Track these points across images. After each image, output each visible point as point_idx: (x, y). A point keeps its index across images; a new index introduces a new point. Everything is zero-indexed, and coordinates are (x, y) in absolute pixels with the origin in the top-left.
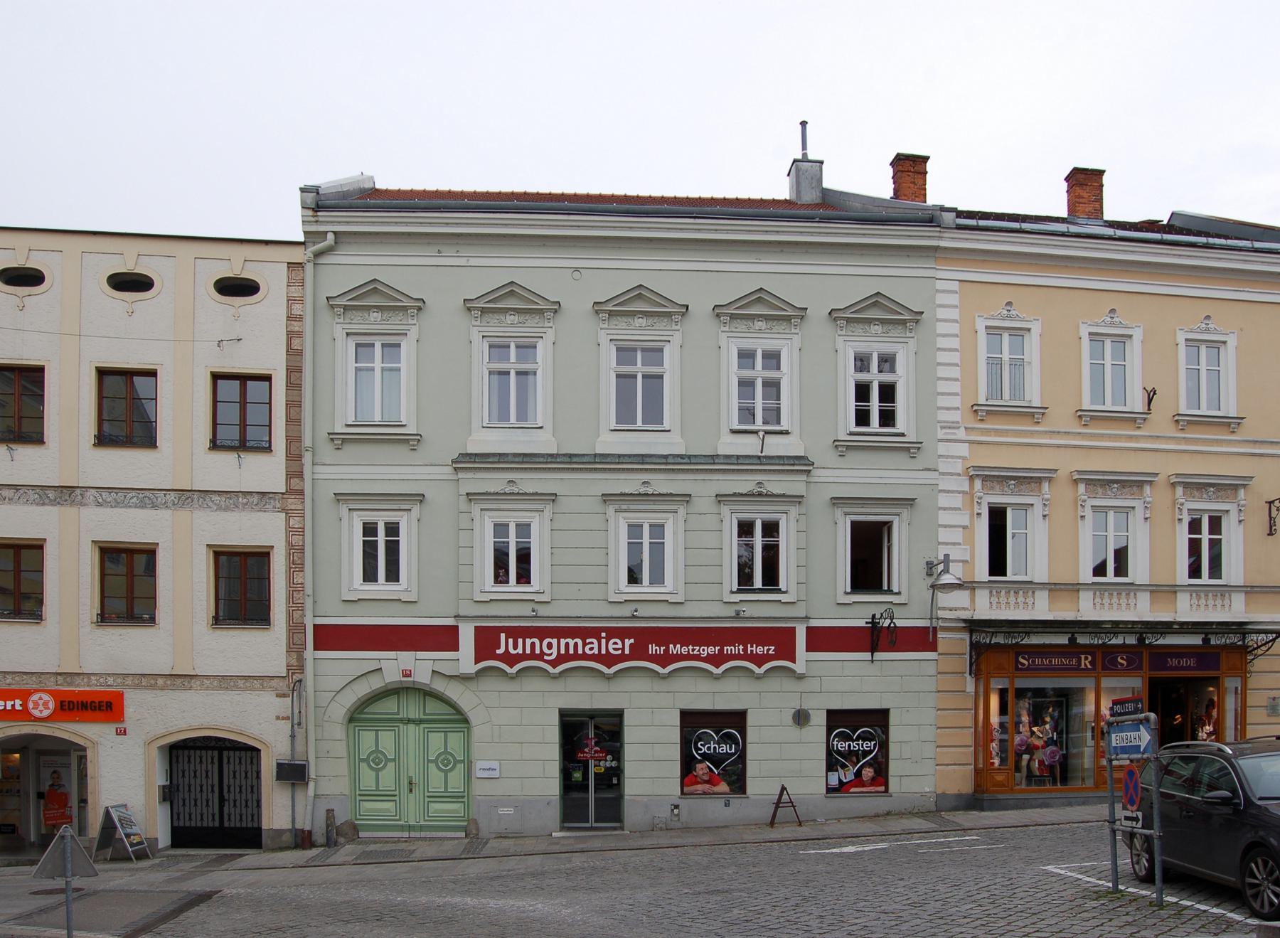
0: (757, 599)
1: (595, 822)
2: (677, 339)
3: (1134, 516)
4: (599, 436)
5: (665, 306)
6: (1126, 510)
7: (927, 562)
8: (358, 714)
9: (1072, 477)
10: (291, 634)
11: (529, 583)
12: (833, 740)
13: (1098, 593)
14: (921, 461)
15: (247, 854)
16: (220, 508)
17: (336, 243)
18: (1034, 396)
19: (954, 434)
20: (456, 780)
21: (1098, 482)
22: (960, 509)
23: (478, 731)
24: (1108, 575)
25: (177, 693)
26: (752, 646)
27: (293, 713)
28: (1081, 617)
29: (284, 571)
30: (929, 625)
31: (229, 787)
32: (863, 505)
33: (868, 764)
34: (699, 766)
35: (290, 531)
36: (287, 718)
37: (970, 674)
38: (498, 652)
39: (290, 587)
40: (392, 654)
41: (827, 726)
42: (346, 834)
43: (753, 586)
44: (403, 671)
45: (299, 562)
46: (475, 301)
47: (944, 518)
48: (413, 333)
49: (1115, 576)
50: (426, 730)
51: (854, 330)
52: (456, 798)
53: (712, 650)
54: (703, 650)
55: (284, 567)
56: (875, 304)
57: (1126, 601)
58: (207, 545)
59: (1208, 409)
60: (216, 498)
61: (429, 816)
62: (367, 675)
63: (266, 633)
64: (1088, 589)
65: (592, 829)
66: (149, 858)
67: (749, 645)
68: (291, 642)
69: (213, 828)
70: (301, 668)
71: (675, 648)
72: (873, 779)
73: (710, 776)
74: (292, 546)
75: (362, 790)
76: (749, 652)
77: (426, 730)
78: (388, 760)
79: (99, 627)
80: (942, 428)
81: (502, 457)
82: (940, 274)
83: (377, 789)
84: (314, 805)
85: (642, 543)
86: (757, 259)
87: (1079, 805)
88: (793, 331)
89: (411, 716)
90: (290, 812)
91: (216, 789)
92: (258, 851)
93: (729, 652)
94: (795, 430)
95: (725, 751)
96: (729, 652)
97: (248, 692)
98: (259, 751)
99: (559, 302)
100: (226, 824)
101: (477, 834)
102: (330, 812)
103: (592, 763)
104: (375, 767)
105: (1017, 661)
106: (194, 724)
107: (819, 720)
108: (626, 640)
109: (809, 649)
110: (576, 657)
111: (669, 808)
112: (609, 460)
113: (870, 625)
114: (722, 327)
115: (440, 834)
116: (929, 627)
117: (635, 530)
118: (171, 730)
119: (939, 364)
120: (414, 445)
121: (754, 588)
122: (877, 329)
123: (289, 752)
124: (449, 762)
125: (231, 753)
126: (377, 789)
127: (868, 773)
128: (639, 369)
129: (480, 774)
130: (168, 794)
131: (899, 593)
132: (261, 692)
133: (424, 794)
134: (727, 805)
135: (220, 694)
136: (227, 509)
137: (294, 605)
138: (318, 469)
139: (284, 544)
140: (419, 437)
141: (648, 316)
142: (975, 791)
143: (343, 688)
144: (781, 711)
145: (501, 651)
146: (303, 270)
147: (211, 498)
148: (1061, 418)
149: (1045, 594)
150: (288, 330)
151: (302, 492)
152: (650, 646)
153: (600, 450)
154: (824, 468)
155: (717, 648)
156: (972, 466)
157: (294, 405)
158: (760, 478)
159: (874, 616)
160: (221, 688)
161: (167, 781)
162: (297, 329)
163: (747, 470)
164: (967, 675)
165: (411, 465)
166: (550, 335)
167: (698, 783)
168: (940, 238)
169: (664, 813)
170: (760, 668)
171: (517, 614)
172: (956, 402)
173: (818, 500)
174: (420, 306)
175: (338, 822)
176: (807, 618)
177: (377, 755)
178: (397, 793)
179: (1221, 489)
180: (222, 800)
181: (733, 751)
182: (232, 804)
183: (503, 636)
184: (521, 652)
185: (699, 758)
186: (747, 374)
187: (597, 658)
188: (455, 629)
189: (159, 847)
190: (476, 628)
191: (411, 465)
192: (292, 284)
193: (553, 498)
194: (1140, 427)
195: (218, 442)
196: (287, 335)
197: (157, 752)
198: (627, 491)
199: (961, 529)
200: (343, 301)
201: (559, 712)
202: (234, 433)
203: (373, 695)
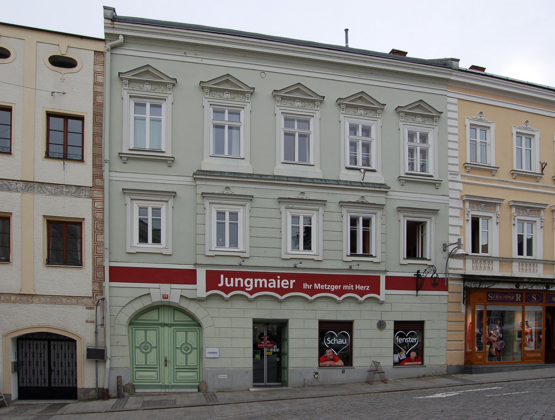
0: (361, 260)
1: (267, 382)
2: (318, 115)
3: (535, 225)
4: (276, 166)
6: (532, 223)
7: (444, 244)
8: (134, 320)
9: (509, 204)
10: (95, 272)
11: (311, 249)
12: (396, 338)
13: (521, 263)
14: (441, 191)
15: (69, 403)
16: (51, 194)
17: (124, 42)
18: (492, 161)
19: (456, 178)
20: (192, 359)
21: (522, 207)
22: (458, 217)
23: (207, 331)
24: (533, 255)
25: (24, 306)
26: (358, 286)
27: (96, 319)
28: (514, 275)
29: (91, 234)
30: (445, 277)
31: (54, 363)
32: (413, 212)
33: (413, 350)
34: (328, 351)
35: (95, 210)
36: (93, 322)
37: (463, 303)
38: (219, 285)
39: (95, 244)
40: (157, 285)
41: (394, 330)
42: (129, 391)
44: (163, 295)
45: (100, 229)
46: (207, 83)
47: (452, 221)
48: (170, 99)
49: (527, 255)
50: (175, 330)
51: (408, 119)
52: (192, 369)
53: (337, 287)
54: (332, 287)
55: (91, 231)
56: (418, 106)
57: (533, 268)
58: (43, 216)
59: (526, 169)
60: (49, 187)
61: (176, 380)
62: (141, 297)
63: (80, 270)
64: (517, 261)
65: (265, 386)
66: (6, 406)
67: (356, 285)
69: (45, 387)
70: (102, 292)
71: (317, 286)
72: (416, 358)
73: (334, 357)
74: (96, 219)
75: (137, 365)
76: (356, 289)
77: (175, 330)
78: (152, 347)
79: (48, 267)
80: (450, 174)
81: (222, 174)
82: (449, 94)
84: (110, 373)
85: (160, 220)
86: (359, 76)
87: (515, 370)
88: (316, 109)
89: (166, 322)
90: (95, 378)
91: (47, 364)
92: (75, 401)
93: (346, 289)
94: (379, 169)
95: (341, 343)
96: (346, 289)
97: (68, 306)
98: (75, 341)
99: (176, 79)
100: (53, 385)
101: (206, 390)
102: (119, 378)
103: (265, 350)
105: (488, 297)
106: (35, 325)
107: (390, 326)
108: (291, 281)
109: (387, 288)
110: (263, 289)
111: (313, 374)
112: (282, 179)
113: (416, 276)
114: (341, 111)
115: (183, 390)
116: (445, 278)
117: (221, 215)
118: (20, 328)
119: (449, 141)
120: (170, 164)
121: (370, 254)
123: (94, 342)
124: (188, 349)
125: (56, 343)
127: (413, 355)
128: (296, 129)
129: (208, 355)
130: (17, 367)
131: (430, 260)
132: (77, 306)
134: (343, 372)
135: (51, 306)
136: (55, 194)
137: (97, 254)
138: (113, 174)
139: (91, 217)
140: (173, 159)
141: (365, 109)
142: (465, 363)
143: (127, 304)
144: (371, 321)
146: (104, 56)
147: (46, 187)
148: (504, 174)
149: (498, 263)
150: (94, 90)
151: (102, 188)
152: (304, 284)
153: (276, 173)
154: (394, 191)
155: (340, 286)
156: (513, 201)
157: (98, 135)
158: (363, 194)
159: (418, 272)
160: (51, 303)
161: (16, 359)
162: (99, 90)
163: (356, 189)
164: (462, 304)
166: (248, 107)
167: (327, 360)
168: (451, 75)
169: (310, 377)
170: (282, 296)
171: (231, 264)
172: (456, 161)
173: (391, 207)
174: (174, 83)
175: (124, 384)
176: (386, 271)
177: (146, 344)
178: (158, 366)
179: (488, 205)
180: (50, 371)
181: (346, 343)
182: (56, 373)
183: (222, 276)
184: (232, 286)
185: (328, 346)
186: (289, 130)
187: (275, 290)
188: (194, 272)
189: (12, 400)
190: (207, 271)
192: (97, 64)
193: (250, 198)
194: (538, 181)
195: (50, 154)
196: (94, 93)
197: (10, 341)
198: (292, 197)
199: (459, 228)
200: (129, 76)
201: (253, 320)
202: (61, 149)
203: (145, 309)
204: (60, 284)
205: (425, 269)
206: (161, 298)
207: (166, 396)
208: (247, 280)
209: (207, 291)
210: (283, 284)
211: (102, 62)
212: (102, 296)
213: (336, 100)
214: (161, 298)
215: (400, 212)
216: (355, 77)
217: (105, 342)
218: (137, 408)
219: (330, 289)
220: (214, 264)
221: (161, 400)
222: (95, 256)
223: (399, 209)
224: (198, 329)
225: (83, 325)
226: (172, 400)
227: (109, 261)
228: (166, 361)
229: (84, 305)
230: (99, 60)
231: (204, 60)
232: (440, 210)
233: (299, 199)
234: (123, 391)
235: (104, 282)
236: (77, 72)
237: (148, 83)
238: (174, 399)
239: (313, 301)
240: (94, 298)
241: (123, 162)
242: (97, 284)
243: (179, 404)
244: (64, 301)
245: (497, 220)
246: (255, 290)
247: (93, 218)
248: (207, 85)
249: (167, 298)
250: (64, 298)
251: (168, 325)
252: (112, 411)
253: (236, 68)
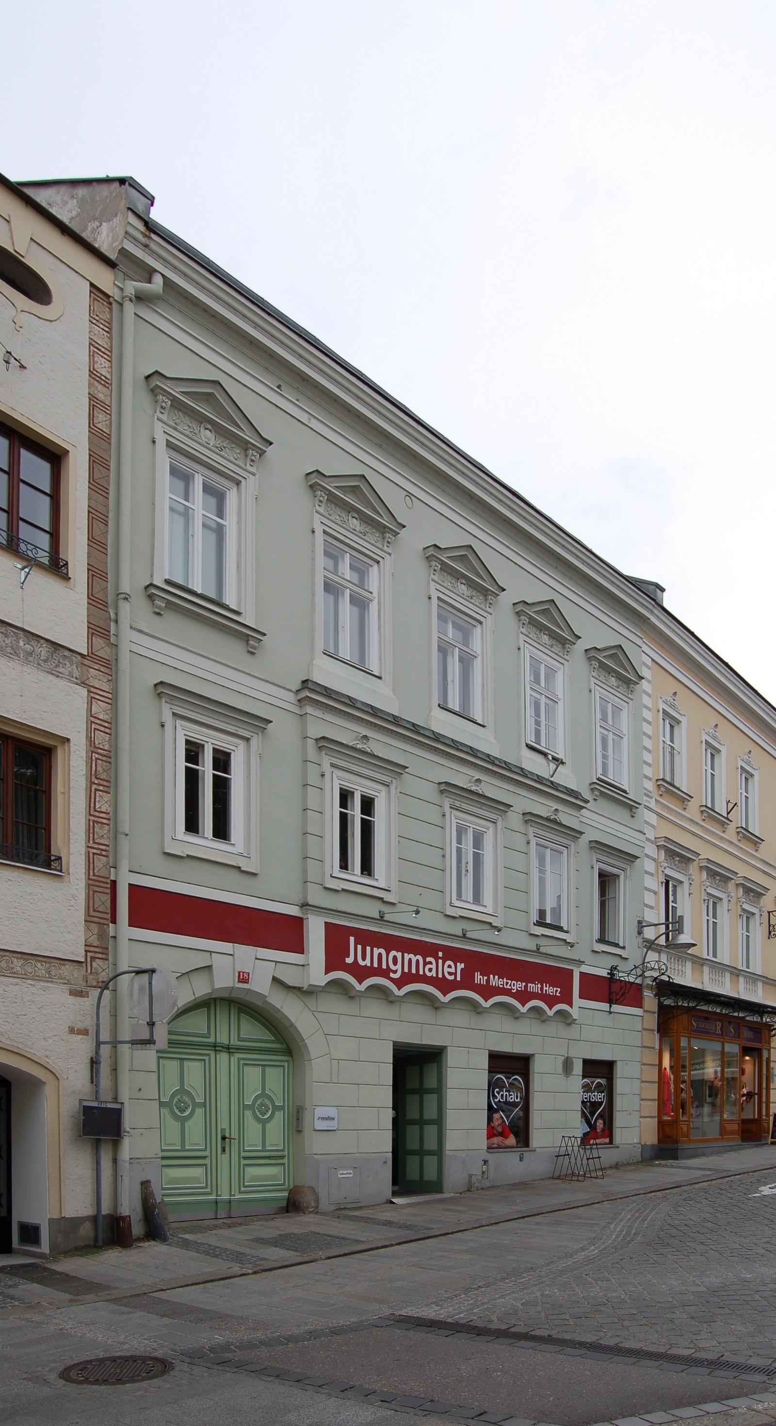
5: (484, 580)
10: (91, 893)
26: (546, 987)
36: (85, 1032)
44: (239, 973)
45: (104, 776)
68: (91, 906)
77: (242, 1062)
83: (183, 1149)
94: (489, 722)
97: (30, 982)
101: (317, 1207)
104: (179, 1114)
107: (578, 1068)
122: (545, 639)
129: (320, 1125)
131: (624, 948)
132: (49, 984)
133: (239, 1154)
137: (96, 846)
142: (659, 1141)
145: (349, 960)
152: (476, 973)
156: (708, 859)
159: (614, 968)
164: (656, 1032)
165: (249, 674)
168: (652, 612)
183: (352, 939)
191: (249, 674)
200: (176, 391)
201: (394, 1046)
204: (10, 916)
205: (635, 965)
206: (234, 980)
208: (393, 953)
209: (327, 971)
210: (446, 970)
211: (105, 321)
212: (106, 962)
213: (307, 472)
214: (234, 980)
215: (592, 851)
216: (460, 513)
219: (510, 987)
222: (90, 850)
223: (594, 845)
224: (287, 1061)
225: (62, 1040)
228: (224, 1138)
229: (65, 984)
230: (98, 314)
231: (313, 420)
232: (639, 858)
233: (471, 791)
236: (51, 321)
237: (210, 427)
239: (321, 989)
240: (86, 965)
241: (156, 610)
242: (95, 929)
244: (19, 969)
245: (690, 890)
246: (406, 979)
247: (88, 743)
248: (326, 484)
250: (17, 958)
253: (372, 471)
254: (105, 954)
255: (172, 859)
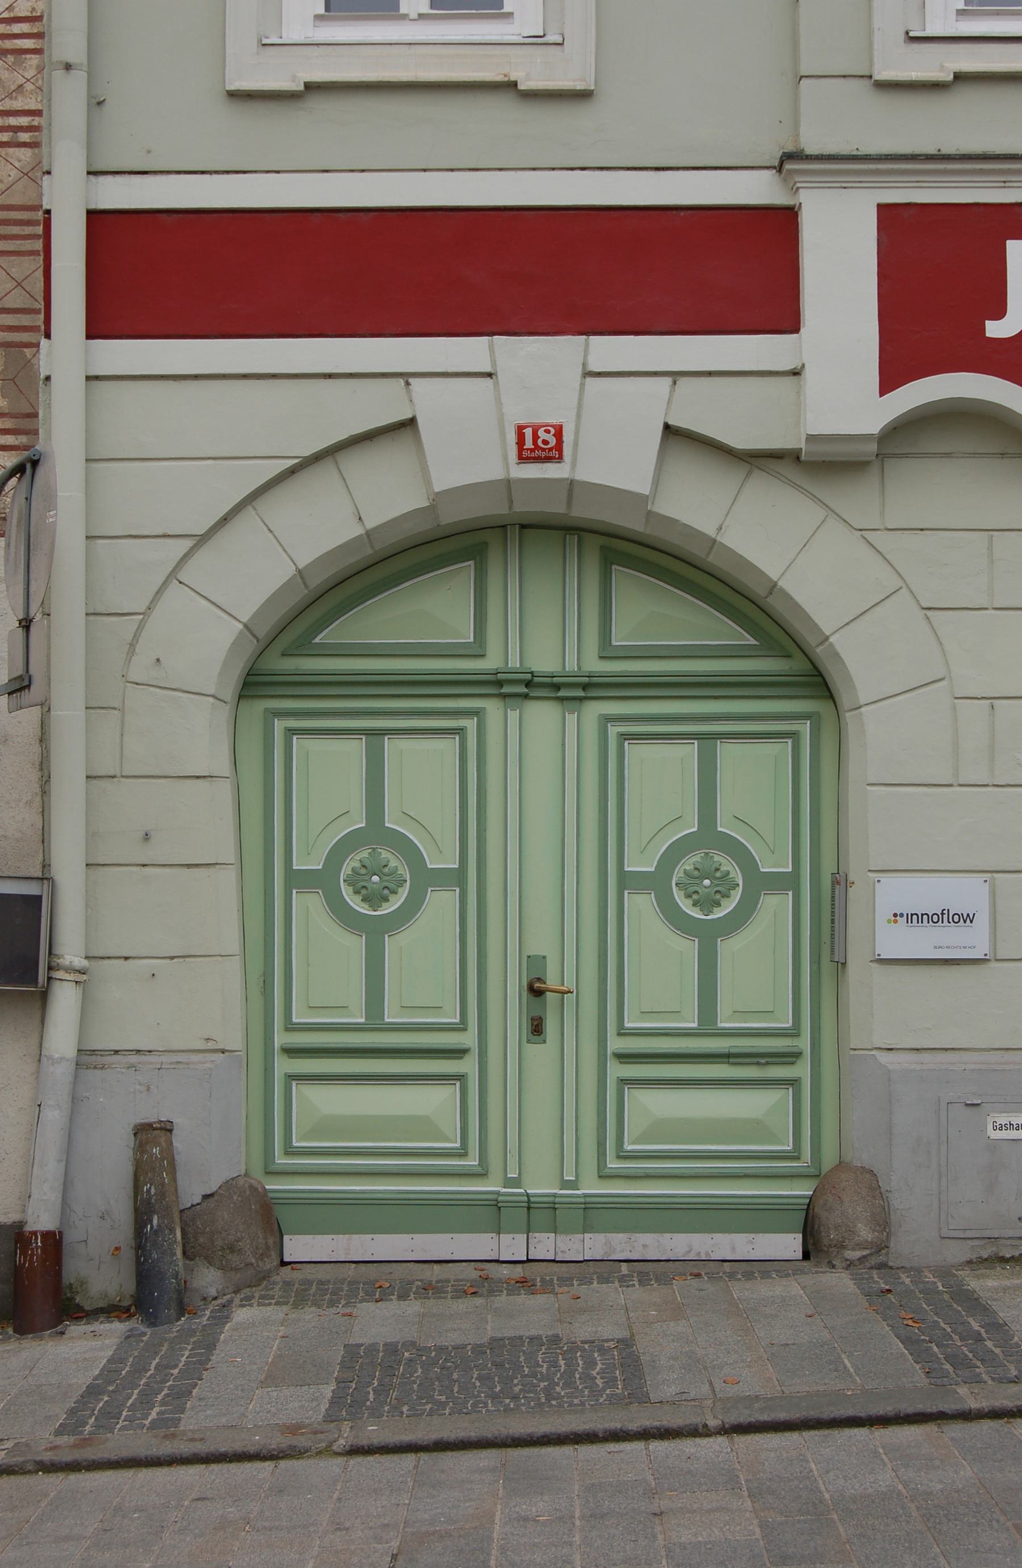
42: (232, 1249)
43: (502, 8)
44: (520, 430)
50: (613, 730)
61: (622, 1156)
77: (613, 730)
83: (375, 1022)
84: (75, 1100)
101: (880, 1247)
104: (696, 914)
124: (724, 886)
126: (375, 1022)
190: (887, 214)
207: (541, 1299)
209: (889, 382)
217: (45, 838)
218: (293, 1429)
220: (949, 148)
221: (496, 1343)
226: (598, 1345)
227: (89, 173)
228: (536, 991)
234: (179, 1252)
235: (44, 342)
238: (610, 1330)
243: (670, 1391)
249: (554, 454)
251: (557, 687)
252: (67, 1457)
254: (26, 432)
255: (260, 107)
